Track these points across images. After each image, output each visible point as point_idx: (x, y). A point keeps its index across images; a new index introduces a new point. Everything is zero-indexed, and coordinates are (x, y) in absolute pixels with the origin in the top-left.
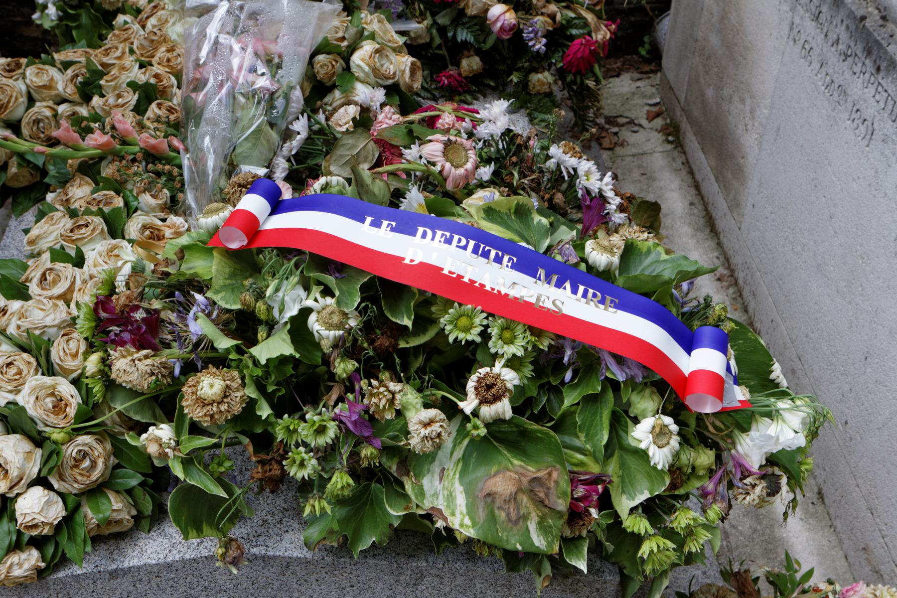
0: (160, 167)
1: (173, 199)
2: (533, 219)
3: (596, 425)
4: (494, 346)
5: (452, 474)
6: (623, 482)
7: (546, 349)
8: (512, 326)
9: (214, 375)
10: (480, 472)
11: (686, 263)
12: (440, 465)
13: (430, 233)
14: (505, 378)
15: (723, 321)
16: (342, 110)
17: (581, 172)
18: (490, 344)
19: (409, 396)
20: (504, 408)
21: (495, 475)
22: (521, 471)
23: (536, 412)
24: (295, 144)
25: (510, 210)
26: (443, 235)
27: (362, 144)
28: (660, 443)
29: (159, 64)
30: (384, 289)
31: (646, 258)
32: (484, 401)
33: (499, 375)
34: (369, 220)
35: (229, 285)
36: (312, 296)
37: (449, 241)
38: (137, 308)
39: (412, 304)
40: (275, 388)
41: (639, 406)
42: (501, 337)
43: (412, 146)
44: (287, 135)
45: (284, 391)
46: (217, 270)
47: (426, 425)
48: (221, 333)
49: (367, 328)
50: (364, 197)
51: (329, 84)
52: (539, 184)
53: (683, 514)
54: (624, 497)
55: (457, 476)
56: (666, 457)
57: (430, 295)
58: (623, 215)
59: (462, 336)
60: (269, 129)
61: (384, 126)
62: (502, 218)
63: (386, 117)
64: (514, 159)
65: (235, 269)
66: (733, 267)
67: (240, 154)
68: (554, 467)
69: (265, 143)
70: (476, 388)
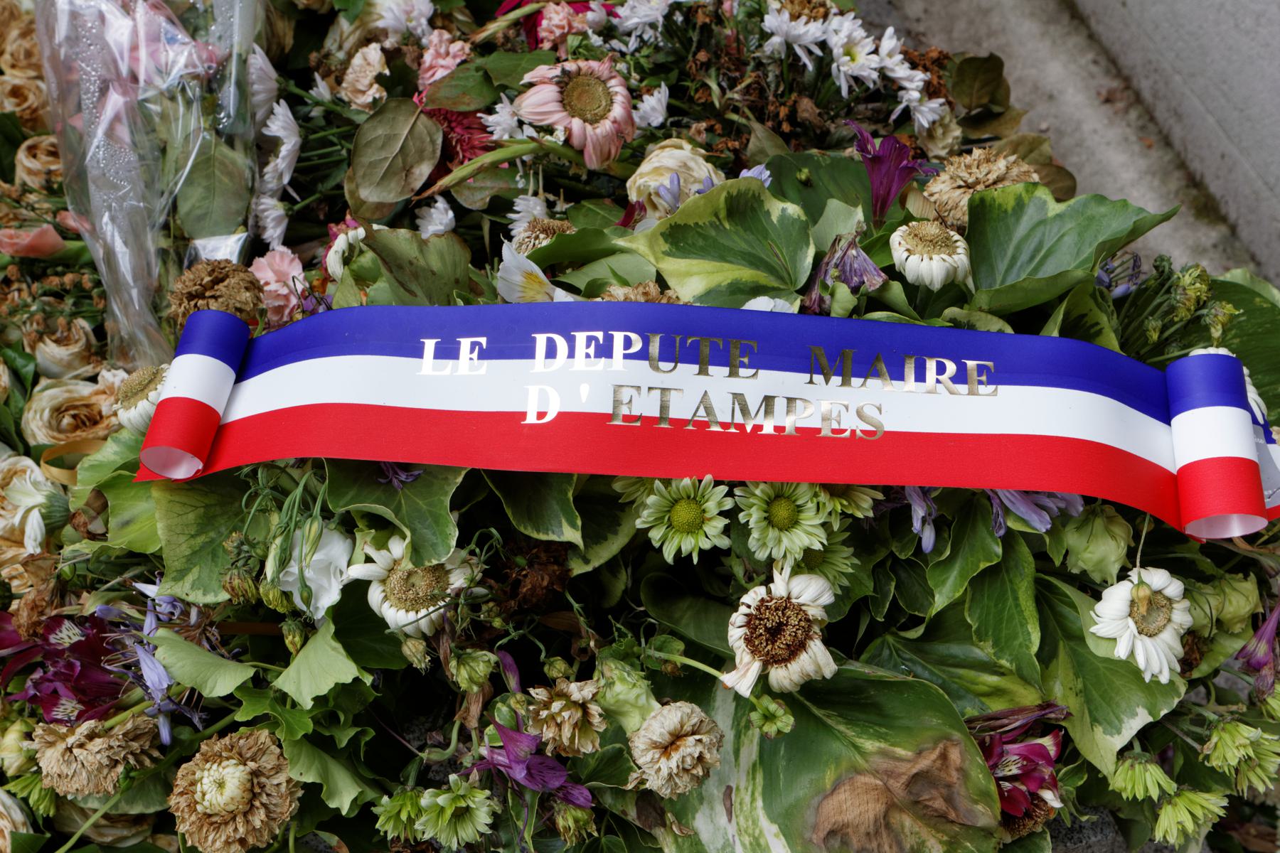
0: (54, 282)
1: (100, 332)
2: (768, 213)
3: (1011, 618)
4: (760, 544)
5: (747, 799)
6: (1088, 701)
7: (871, 514)
8: (787, 491)
9: (218, 758)
10: (802, 788)
11: (1103, 209)
12: (721, 781)
13: (561, 342)
14: (801, 601)
15: (1204, 305)
16: (357, 60)
17: (836, 43)
18: (752, 543)
19: (619, 687)
20: (817, 659)
21: (835, 788)
22: (884, 764)
23: (881, 619)
24: (281, 166)
25: (716, 215)
26: (590, 339)
27: (406, 126)
28: (1152, 627)
29: (13, 66)
30: (498, 490)
31: (1018, 220)
32: (771, 660)
33: (789, 598)
34: (430, 345)
35: (202, 548)
36: (359, 556)
37: (605, 351)
38: (56, 622)
39: (570, 495)
40: (352, 732)
41: (1087, 555)
42: (769, 521)
43: (498, 107)
44: (265, 148)
45: (372, 733)
46: (169, 529)
47: (667, 748)
48: (212, 658)
49: (495, 571)
50: (414, 287)
51: (324, 10)
52: (762, 91)
53: (1226, 736)
54: (1099, 730)
55: (760, 803)
56: (1171, 648)
57: (599, 469)
58: (936, 103)
59: (689, 544)
60: (225, 150)
61: (440, 73)
62: (705, 237)
63: (438, 55)
64: (702, 56)
65: (206, 506)
66: (1126, 72)
67: (188, 214)
68: (948, 738)
69: (226, 180)
70: (748, 641)
